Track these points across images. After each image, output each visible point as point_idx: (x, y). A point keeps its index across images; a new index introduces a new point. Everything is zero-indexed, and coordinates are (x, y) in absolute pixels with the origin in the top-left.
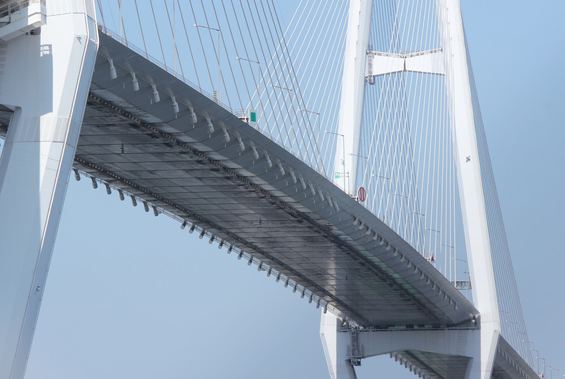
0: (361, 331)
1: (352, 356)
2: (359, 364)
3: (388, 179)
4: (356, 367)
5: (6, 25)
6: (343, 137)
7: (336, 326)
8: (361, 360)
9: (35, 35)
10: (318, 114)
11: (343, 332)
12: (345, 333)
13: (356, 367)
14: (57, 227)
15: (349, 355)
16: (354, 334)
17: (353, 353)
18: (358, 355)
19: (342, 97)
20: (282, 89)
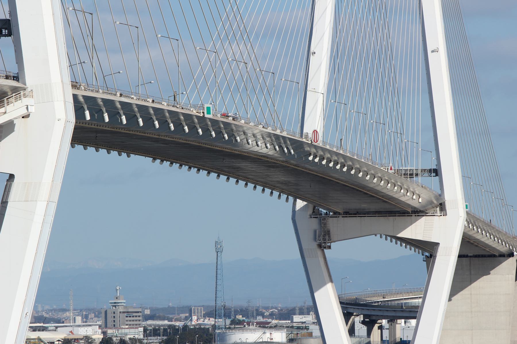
0: (331, 217)
1: (322, 241)
2: (329, 247)
3: (245, 63)
4: (326, 251)
5: (3, 115)
6: (137, 28)
7: (366, 330)
8: (331, 244)
9: (25, 119)
10: (215, 52)
11: (314, 217)
12: (316, 218)
13: (326, 251)
14: (142, 154)
15: (320, 241)
16: (324, 220)
17: (323, 239)
18: (329, 241)
19: (328, 65)
20: (243, 61)
